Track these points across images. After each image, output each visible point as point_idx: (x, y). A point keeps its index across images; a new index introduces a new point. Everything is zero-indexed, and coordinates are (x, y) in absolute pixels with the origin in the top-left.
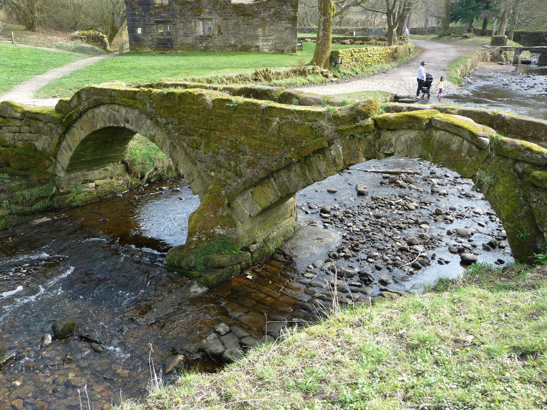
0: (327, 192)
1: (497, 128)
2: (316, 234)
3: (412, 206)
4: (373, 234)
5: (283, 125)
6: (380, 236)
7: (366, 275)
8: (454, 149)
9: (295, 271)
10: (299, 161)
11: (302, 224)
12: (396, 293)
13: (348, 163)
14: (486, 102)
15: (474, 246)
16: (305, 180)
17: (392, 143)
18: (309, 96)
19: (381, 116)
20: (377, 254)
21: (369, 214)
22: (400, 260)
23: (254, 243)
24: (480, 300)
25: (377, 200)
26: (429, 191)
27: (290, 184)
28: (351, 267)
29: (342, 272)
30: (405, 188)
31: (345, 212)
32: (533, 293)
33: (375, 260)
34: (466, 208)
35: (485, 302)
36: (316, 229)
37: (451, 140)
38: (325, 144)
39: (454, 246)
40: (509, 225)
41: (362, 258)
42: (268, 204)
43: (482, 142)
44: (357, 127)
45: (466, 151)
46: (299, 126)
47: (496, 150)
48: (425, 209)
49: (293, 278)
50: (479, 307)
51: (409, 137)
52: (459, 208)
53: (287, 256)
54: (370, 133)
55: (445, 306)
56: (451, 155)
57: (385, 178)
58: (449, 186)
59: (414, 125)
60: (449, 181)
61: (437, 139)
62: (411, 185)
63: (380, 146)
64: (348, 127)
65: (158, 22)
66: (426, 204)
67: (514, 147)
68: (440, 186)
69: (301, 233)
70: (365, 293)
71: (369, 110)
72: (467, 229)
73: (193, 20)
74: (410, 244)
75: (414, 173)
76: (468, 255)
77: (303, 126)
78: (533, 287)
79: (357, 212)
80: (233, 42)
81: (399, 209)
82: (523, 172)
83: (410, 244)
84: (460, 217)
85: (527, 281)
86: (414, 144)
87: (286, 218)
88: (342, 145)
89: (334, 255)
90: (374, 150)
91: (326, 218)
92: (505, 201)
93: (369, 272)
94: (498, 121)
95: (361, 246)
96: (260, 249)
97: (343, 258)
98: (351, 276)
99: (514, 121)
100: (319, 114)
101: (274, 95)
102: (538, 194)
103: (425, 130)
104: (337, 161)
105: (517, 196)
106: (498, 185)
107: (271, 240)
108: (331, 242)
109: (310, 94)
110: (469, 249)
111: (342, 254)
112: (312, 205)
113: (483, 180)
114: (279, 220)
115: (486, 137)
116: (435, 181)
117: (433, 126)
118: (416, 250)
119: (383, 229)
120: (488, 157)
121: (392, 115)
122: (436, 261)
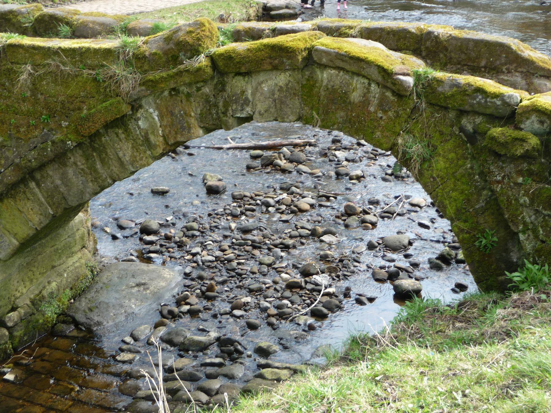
0: (151, 194)
1: (427, 55)
2: (133, 276)
3: (304, 204)
4: (239, 264)
5: (41, 78)
6: (251, 265)
7: (231, 342)
8: (356, 101)
9: (99, 352)
10: (79, 145)
11: (105, 260)
12: (286, 368)
13: (171, 141)
14: (419, 8)
15: (415, 265)
16: (95, 180)
17: (247, 99)
18: (90, 19)
19: (222, 49)
20: (249, 299)
21: (230, 228)
22: (290, 305)
23: (13, 309)
24: (421, 369)
25: (242, 199)
26: (333, 174)
27: (69, 190)
28: (203, 330)
29: (187, 342)
30: (290, 172)
31: (185, 227)
32: (508, 346)
33: (245, 311)
34: (396, 198)
35: (430, 373)
36: (133, 267)
37: (349, 84)
38: (126, 109)
39: (382, 268)
40: (461, 225)
41: (222, 311)
42: (31, 232)
43: (401, 83)
44: (180, 74)
45: (376, 102)
46: (73, 79)
47: (426, 97)
48: (327, 207)
49: (95, 367)
50: (420, 384)
51: (276, 85)
52: (385, 199)
53: (82, 324)
54: (205, 81)
55: (361, 391)
56: (352, 111)
57: (254, 157)
58: (365, 161)
59: (283, 63)
60: (365, 152)
61: (324, 84)
62: (301, 167)
63: (227, 105)
64: (164, 74)
66: (328, 198)
67: (455, 89)
68: (351, 163)
69: (105, 277)
70: (230, 377)
71: (199, 39)
72: (400, 236)
74: (306, 273)
75: (305, 145)
76: (406, 283)
77: (80, 78)
78: (508, 334)
79: (207, 226)
81: (282, 213)
82: (475, 132)
83: (306, 273)
84: (388, 214)
85: (497, 325)
86: (286, 97)
87: (73, 254)
88: (158, 108)
89: (171, 312)
90: (217, 113)
91: (151, 243)
92: (450, 184)
93: (238, 338)
94: (428, 43)
95: (218, 288)
96: (26, 319)
97: (188, 316)
98: (203, 347)
99: (454, 42)
100: (108, 52)
101: (23, 20)
102: (502, 168)
103: (302, 69)
104: (152, 138)
105: (469, 175)
106: (436, 158)
107: (47, 299)
108: (163, 288)
109: (91, 14)
110: (407, 271)
111: (186, 308)
112: (124, 222)
113: (410, 151)
114: (60, 257)
115: (408, 75)
116: (341, 154)
117: (315, 62)
118: (317, 285)
119: (257, 252)
120: (415, 109)
121: (241, 47)
122: (352, 300)
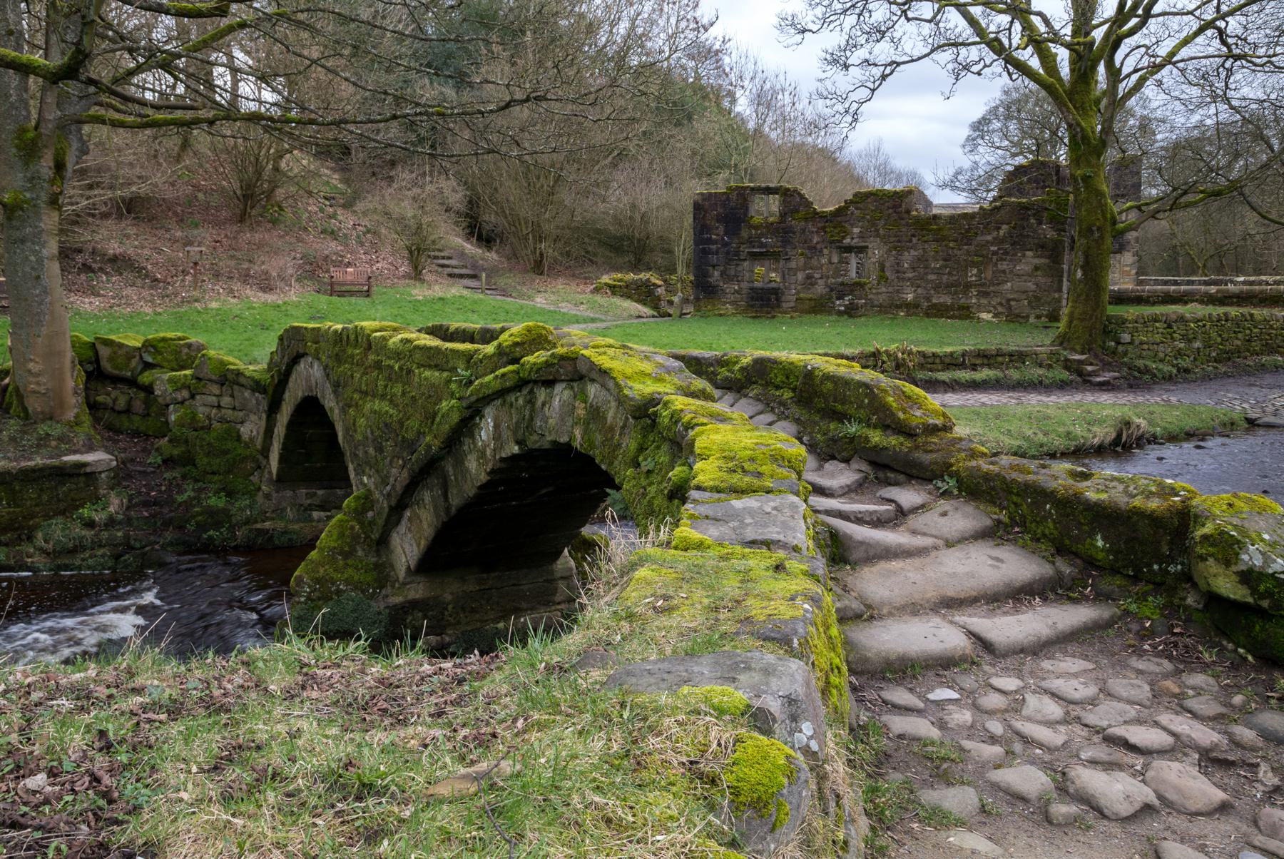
65: (754, 256)
73: (826, 251)
80: (910, 297)
